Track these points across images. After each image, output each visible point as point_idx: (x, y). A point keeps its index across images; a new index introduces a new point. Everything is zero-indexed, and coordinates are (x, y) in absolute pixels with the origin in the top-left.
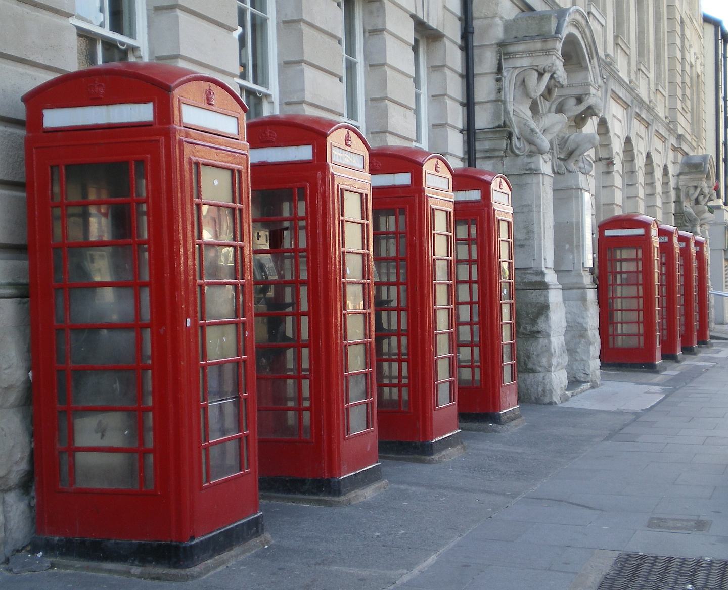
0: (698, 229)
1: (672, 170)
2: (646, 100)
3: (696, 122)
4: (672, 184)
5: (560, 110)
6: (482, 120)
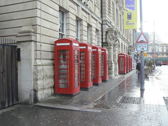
0: (131, 55)
1: (127, 46)
2: (124, 37)
3: (130, 40)
4: (127, 49)
5: (114, 40)
6: (104, 41)
